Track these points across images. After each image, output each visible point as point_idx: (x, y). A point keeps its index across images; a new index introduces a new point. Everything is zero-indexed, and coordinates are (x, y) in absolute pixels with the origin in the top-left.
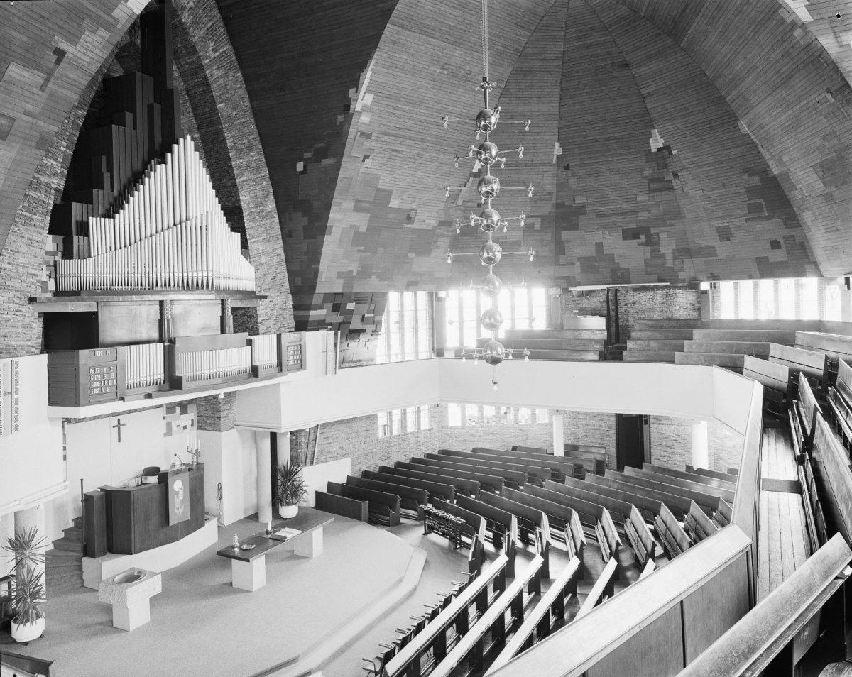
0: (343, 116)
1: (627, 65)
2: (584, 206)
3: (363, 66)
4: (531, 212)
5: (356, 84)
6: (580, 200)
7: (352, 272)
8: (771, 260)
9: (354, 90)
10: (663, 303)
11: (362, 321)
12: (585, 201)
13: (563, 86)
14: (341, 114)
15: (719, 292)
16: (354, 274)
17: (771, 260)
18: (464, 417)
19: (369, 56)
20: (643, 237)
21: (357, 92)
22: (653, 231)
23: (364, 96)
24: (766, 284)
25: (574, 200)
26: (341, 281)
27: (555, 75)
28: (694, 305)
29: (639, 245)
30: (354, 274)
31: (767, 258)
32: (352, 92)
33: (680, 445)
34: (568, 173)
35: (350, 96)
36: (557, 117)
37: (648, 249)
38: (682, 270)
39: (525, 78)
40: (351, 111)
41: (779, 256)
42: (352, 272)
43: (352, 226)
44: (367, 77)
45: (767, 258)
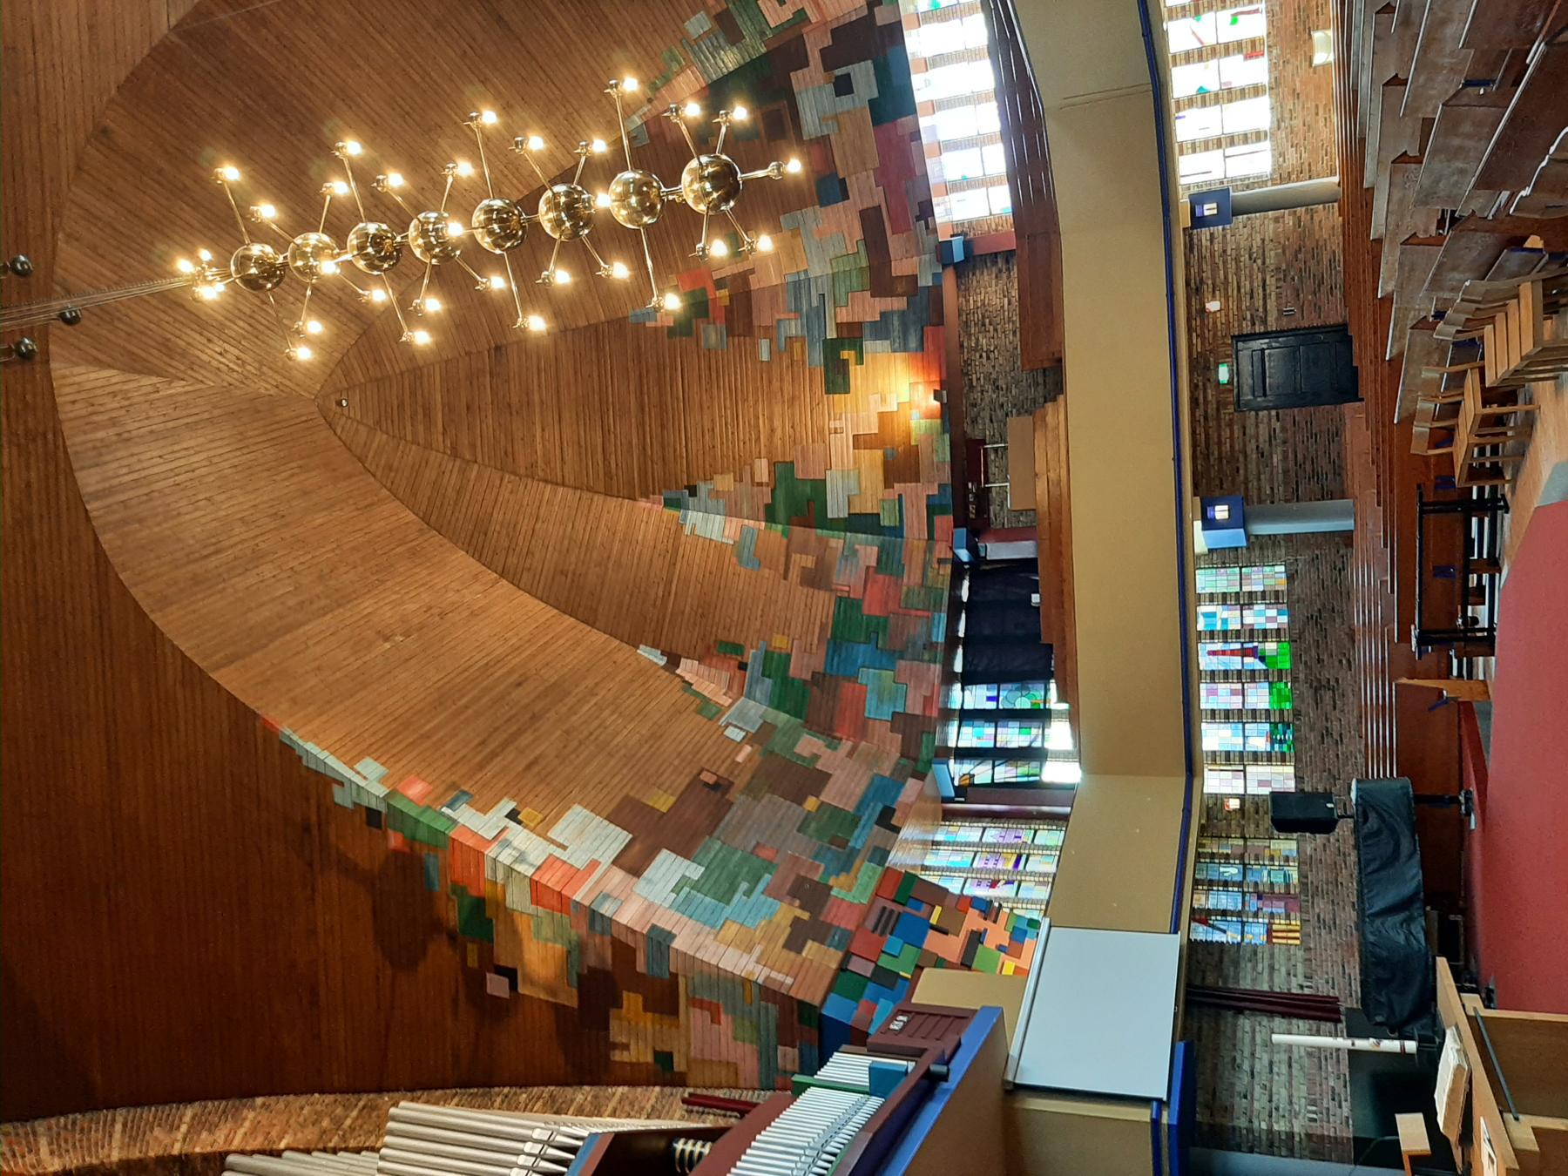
0: (391, 832)
1: (497, 348)
2: (773, 465)
3: (289, 754)
4: (776, 570)
5: (324, 781)
6: (762, 470)
7: (796, 920)
8: (876, 95)
9: (336, 788)
10: (996, 330)
11: (945, 933)
12: (764, 462)
13: (522, 471)
14: (386, 838)
15: (970, 222)
16: (805, 916)
17: (876, 95)
18: (1269, 758)
19: (270, 733)
20: (845, 354)
21: (342, 784)
22: (832, 334)
23: (358, 773)
24: (924, 87)
25: (760, 484)
26: (811, 947)
27: (498, 482)
28: (1000, 271)
29: (860, 361)
30: (805, 916)
31: (871, 102)
32: (341, 797)
33: (1312, 263)
34: (703, 488)
35: (348, 804)
36: (586, 495)
37: (868, 345)
38: (913, 279)
39: (490, 534)
40: (382, 808)
41: (863, 74)
42: (796, 920)
43: (677, 889)
44: (319, 752)
45: (871, 102)
